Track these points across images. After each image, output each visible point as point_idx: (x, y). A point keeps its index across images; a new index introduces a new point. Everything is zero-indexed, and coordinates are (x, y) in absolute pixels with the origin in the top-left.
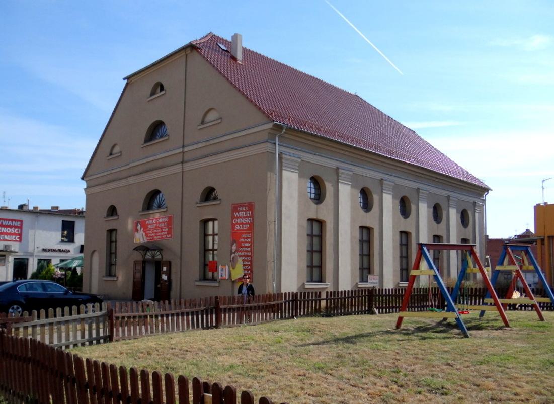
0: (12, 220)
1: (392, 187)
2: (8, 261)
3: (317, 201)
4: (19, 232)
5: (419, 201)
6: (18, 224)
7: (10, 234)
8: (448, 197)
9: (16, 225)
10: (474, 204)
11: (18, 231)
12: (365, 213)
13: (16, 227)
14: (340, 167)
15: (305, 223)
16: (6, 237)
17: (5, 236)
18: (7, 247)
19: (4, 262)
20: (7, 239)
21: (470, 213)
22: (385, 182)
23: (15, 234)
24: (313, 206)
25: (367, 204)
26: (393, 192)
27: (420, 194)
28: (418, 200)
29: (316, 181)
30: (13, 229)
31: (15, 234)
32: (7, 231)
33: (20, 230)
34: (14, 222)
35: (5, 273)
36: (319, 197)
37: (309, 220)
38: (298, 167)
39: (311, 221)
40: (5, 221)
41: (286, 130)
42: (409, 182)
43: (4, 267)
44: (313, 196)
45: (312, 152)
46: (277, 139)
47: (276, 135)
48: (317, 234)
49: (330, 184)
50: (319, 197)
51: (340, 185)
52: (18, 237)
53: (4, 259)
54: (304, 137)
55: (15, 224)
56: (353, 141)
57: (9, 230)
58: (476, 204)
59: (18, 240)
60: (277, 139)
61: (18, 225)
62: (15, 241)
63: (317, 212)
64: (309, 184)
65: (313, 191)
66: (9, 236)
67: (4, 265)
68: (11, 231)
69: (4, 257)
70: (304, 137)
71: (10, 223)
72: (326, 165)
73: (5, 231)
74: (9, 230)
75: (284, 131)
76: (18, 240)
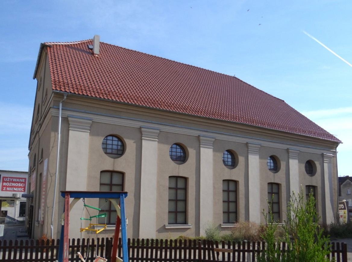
0: (19, 178)
1: (212, 143)
2: (16, 204)
3: (275, 171)
4: (24, 186)
5: (249, 153)
6: (23, 181)
7: (18, 187)
8: (287, 150)
9: (21, 181)
10: (322, 155)
11: (23, 185)
12: (311, 177)
13: (21, 183)
14: (290, 148)
15: (266, 187)
16: (15, 189)
17: (15, 189)
18: (14, 195)
19: (14, 205)
20: (15, 190)
21: (318, 164)
22: (201, 138)
23: (21, 187)
24: (271, 173)
25: (235, 163)
26: (213, 146)
27: (290, 153)
28: (248, 153)
29: (273, 158)
30: (19, 184)
31: (21, 187)
32: (16, 185)
33: (24, 184)
34: (20, 179)
35: (14, 212)
36: (276, 168)
37: (269, 183)
38: (213, 144)
39: (271, 184)
40: (15, 179)
41: (67, 97)
42: (238, 138)
43: (13, 208)
44: (272, 167)
45: (321, 148)
46: (61, 105)
47: (60, 101)
48: (231, 191)
49: (132, 141)
50: (276, 168)
51: (202, 149)
52: (23, 188)
53: (14, 203)
54: (97, 102)
55: (21, 180)
56: (315, 134)
57: (17, 185)
58: (324, 155)
59: (23, 191)
60: (61, 105)
61: (23, 181)
62: (20, 191)
63: (114, 164)
64: (269, 161)
65: (272, 165)
66: (17, 188)
67: (13, 207)
68: (19, 185)
69: (13, 202)
70: (97, 102)
71: (18, 180)
72: (304, 151)
73: (14, 185)
74: (17, 185)
75: (65, 97)
76: (23, 191)
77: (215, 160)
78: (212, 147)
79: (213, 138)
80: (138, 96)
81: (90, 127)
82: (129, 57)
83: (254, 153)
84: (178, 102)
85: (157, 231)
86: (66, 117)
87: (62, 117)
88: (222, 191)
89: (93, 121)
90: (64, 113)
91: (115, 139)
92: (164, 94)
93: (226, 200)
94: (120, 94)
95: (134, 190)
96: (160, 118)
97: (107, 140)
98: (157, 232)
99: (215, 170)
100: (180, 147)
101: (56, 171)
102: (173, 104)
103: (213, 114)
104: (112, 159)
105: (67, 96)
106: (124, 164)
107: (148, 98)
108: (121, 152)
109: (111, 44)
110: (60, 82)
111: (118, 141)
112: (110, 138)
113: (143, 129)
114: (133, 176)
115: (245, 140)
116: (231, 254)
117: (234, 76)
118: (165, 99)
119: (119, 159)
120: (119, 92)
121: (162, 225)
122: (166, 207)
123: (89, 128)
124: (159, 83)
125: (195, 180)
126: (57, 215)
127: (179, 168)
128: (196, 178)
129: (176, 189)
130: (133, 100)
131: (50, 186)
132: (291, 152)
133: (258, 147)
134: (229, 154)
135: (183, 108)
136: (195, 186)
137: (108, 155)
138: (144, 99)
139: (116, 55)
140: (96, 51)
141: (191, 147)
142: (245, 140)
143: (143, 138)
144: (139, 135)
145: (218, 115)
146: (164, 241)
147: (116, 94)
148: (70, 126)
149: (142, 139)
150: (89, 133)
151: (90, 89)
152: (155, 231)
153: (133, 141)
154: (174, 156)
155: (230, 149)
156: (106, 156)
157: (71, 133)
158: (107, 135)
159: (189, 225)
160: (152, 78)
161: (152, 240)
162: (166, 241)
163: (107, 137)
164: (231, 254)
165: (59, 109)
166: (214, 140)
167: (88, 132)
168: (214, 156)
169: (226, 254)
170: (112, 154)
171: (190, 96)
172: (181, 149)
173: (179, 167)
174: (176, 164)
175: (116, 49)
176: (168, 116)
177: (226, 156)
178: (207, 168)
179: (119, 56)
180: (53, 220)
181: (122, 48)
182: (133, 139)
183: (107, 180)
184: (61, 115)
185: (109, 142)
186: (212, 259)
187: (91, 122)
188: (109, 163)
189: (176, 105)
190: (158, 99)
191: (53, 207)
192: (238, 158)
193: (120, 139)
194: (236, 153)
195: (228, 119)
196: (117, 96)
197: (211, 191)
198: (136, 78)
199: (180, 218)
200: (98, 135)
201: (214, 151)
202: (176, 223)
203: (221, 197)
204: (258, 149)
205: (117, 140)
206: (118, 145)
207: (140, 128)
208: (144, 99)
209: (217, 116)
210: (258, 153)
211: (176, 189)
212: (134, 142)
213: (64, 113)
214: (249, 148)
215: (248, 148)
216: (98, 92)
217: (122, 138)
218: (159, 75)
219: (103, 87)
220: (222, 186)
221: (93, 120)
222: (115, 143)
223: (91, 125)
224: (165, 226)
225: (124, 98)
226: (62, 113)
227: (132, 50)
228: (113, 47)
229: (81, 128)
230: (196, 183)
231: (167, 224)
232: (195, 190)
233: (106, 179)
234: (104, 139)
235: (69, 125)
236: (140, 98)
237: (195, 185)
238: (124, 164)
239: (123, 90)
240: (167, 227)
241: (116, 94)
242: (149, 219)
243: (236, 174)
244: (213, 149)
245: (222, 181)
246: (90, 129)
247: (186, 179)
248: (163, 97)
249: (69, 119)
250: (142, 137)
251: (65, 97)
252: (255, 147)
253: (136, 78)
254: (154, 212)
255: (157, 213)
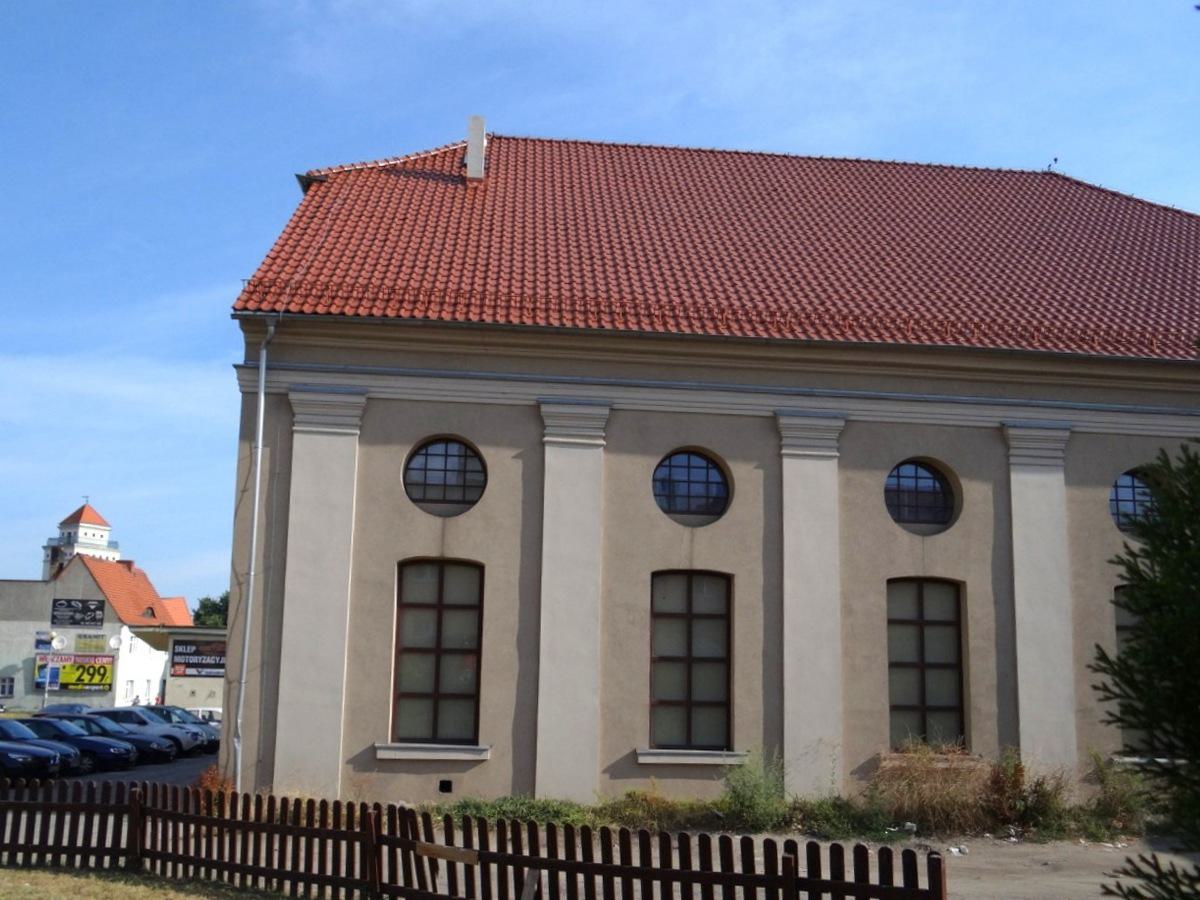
5: (1012, 467)
41: (276, 327)
42: (1160, 420)
54: (377, 334)
63: (443, 536)
77: (846, 504)
78: (838, 454)
79: (835, 417)
80: (905, 315)
81: (362, 418)
82: (856, 182)
83: (1039, 462)
84: (1090, 319)
85: (604, 772)
86: (282, 391)
87: (266, 394)
88: (885, 624)
89: (372, 395)
90: (275, 378)
91: (696, 461)
92: (1031, 297)
93: (910, 656)
94: (845, 318)
95: (517, 627)
96: (1089, 387)
97: (670, 466)
98: (607, 776)
99: (849, 541)
100: (931, 473)
101: (250, 567)
102: (1037, 329)
103: (1142, 343)
104: (438, 521)
105: (278, 325)
106: (482, 534)
107: (988, 320)
108: (716, 504)
109: (740, 150)
110: (722, 311)
111: (707, 468)
112: (682, 459)
113: (783, 421)
114: (514, 576)
115: (992, 416)
116: (477, 869)
117: (1046, 169)
118: (996, 307)
119: (462, 518)
120: (839, 311)
121: (627, 751)
122: (877, 690)
123: (356, 421)
124: (964, 258)
125: (760, 580)
126: (256, 706)
127: (692, 541)
128: (766, 573)
129: (920, 623)
130: (816, 328)
131: (236, 615)
132: (790, 427)
133: (1061, 440)
134: (1137, 484)
135: (1077, 339)
136: (761, 605)
137: (678, 516)
138: (929, 324)
139: (830, 185)
140: (475, 168)
141: (746, 459)
142: (992, 416)
143: (784, 451)
144: (533, 433)
145: (1165, 345)
146: (292, 802)
147: (808, 317)
148: (297, 418)
149: (780, 456)
150: (836, 461)
151: (763, 316)
152: (598, 769)
153: (514, 452)
154: (697, 497)
155: (921, 454)
156: (415, 511)
157: (299, 441)
158: (897, 462)
159: (736, 753)
160: (957, 248)
161: (337, 804)
162: (324, 803)
163: (898, 467)
164: (477, 869)
165: (257, 368)
166: (841, 423)
167: (600, 446)
168: (846, 485)
169: (460, 867)
170: (688, 512)
171: (1088, 294)
172: (935, 478)
173: (693, 535)
174: (681, 527)
175: (805, 166)
176: (626, 351)
177: (1125, 494)
178: (818, 539)
179: (805, 183)
180: (239, 721)
181: (874, 162)
182: (511, 445)
183: (674, 601)
184: (266, 387)
185: (680, 475)
186: (898, 880)
187: (362, 400)
188: (423, 534)
189: (1012, 326)
190: (978, 316)
191: (240, 683)
192: (960, 485)
193: (714, 463)
194: (950, 471)
195: (1152, 351)
196: (837, 326)
197: (832, 622)
198: (888, 248)
199: (704, 721)
200: (387, 440)
201: (844, 464)
202: (434, 738)
203: (877, 649)
204: (1063, 446)
205: (703, 463)
206: (708, 483)
207: (537, 406)
208: (929, 324)
209: (1158, 347)
210: (1060, 462)
211: (920, 623)
212: (515, 457)
213: (275, 378)
214: (1013, 443)
215: (1008, 447)
216: (763, 322)
217: (720, 458)
218: (990, 231)
219: (728, 298)
220: (884, 603)
221: (368, 392)
222: (699, 475)
223: (365, 410)
224: (634, 754)
225: (833, 329)
226: (266, 382)
227: (905, 164)
228: (769, 159)
229: (330, 423)
230: (766, 594)
231: (642, 744)
232: (761, 622)
233: (423, 588)
234: (890, 476)
235: (293, 415)
236: (912, 322)
237: (764, 601)
238: (482, 534)
239: (852, 305)
240: (642, 760)
241: (832, 318)
242: (576, 726)
243: (953, 553)
244: (839, 458)
245: (884, 587)
246: (360, 423)
247: (956, 588)
248: (985, 306)
249: (293, 396)
250: (781, 448)
251: (272, 329)
252: (1046, 439)
253: (888, 248)
254: (591, 700)
255: (605, 705)
